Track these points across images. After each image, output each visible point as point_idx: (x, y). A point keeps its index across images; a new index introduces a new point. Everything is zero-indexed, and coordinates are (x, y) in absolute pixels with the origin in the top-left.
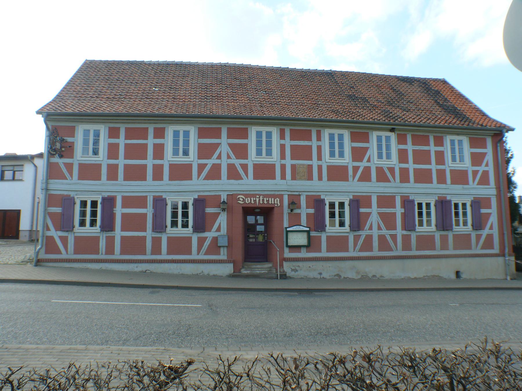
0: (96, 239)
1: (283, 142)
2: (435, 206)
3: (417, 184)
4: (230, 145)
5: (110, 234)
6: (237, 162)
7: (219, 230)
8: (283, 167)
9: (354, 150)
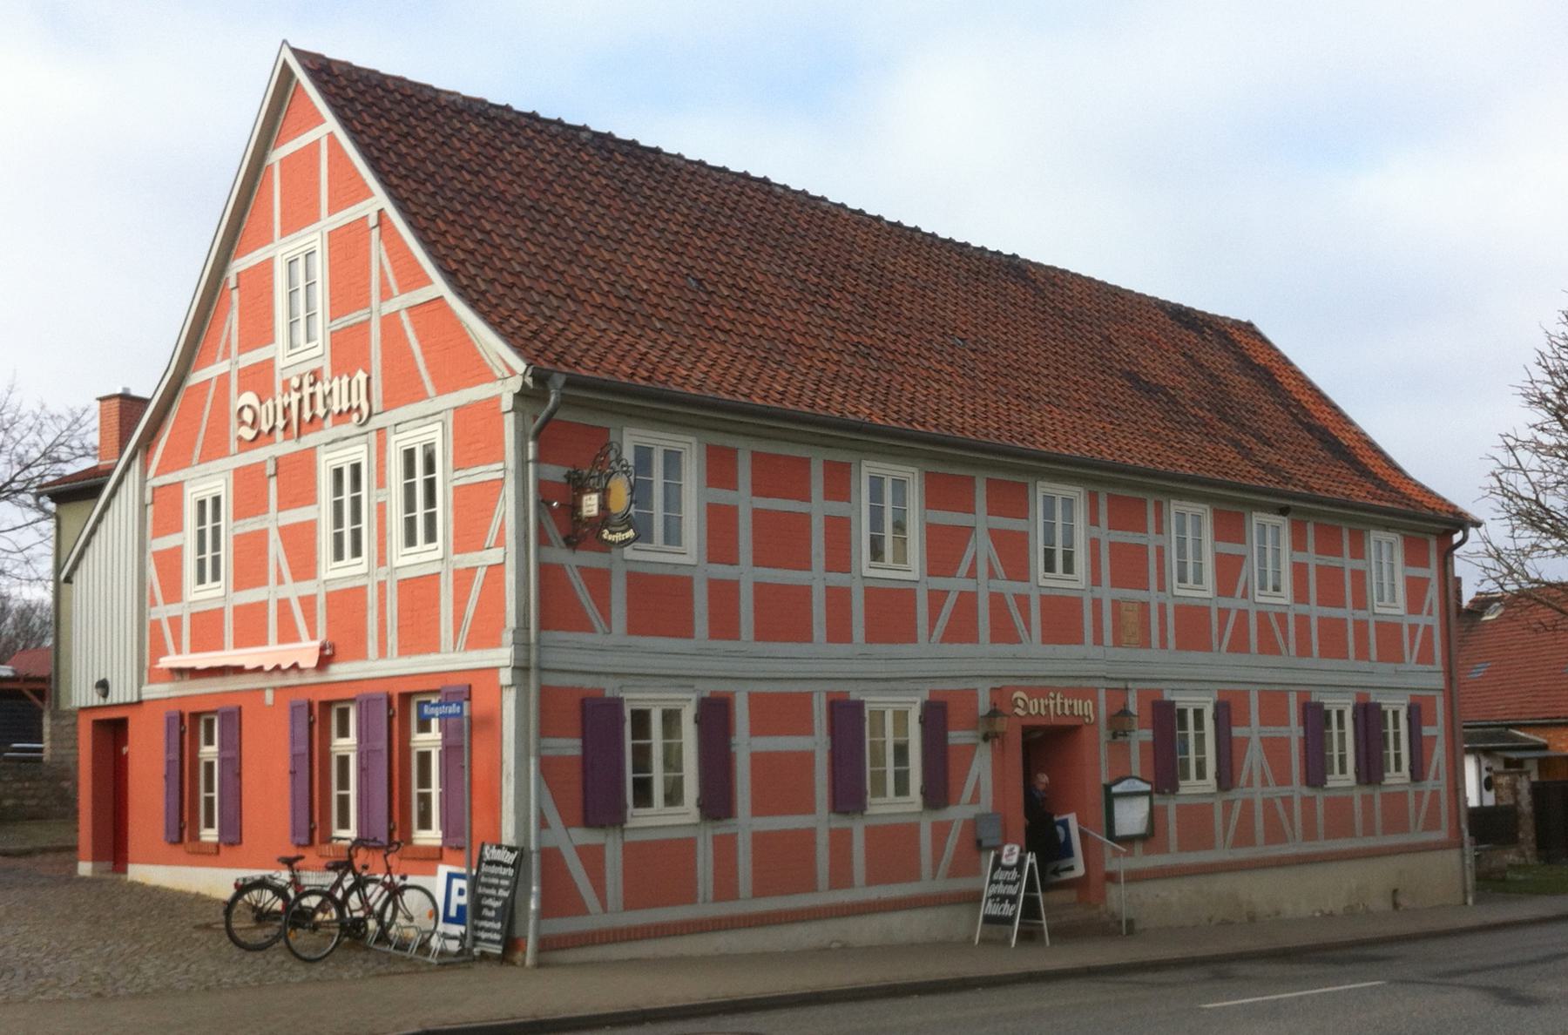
0: (685, 848)
1: (722, 496)
2: (1355, 720)
3: (1327, 661)
4: (994, 534)
5: (723, 829)
6: (1009, 588)
7: (975, 799)
8: (1097, 604)
9: (934, 535)
